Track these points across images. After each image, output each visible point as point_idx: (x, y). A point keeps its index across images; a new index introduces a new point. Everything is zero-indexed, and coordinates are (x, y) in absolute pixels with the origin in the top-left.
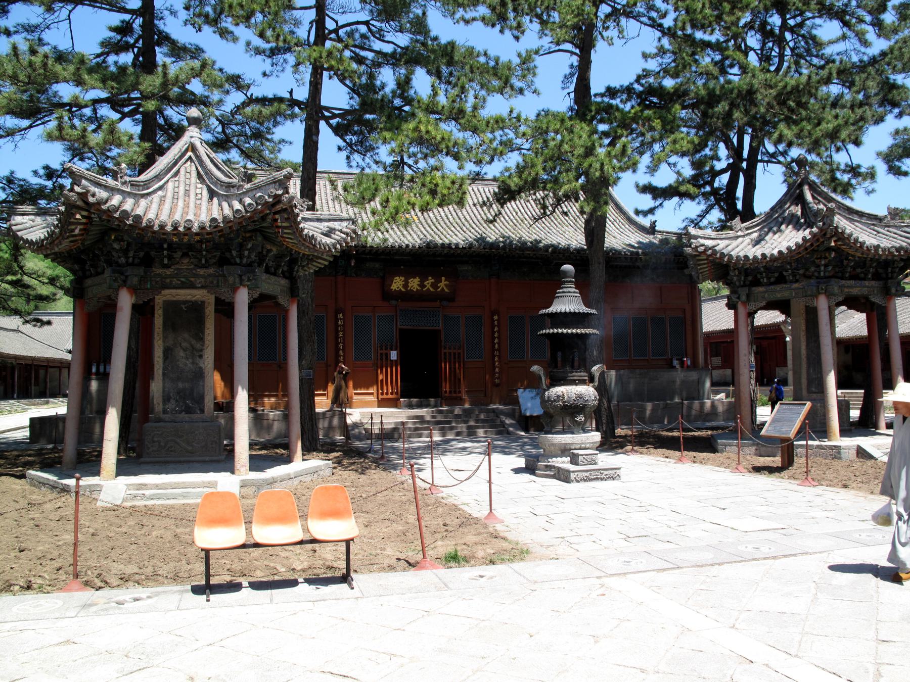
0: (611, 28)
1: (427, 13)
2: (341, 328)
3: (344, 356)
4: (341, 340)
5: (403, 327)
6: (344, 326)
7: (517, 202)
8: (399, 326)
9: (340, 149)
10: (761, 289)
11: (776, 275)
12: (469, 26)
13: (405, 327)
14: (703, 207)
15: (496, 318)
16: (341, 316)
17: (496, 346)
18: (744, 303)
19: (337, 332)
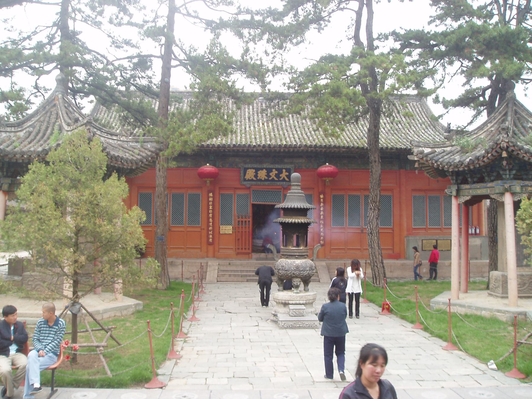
0: (250, 56)
1: (237, 38)
2: (211, 203)
3: (213, 223)
4: (210, 211)
5: (254, 203)
6: (213, 201)
7: (249, 141)
8: (252, 202)
9: (284, 84)
10: (467, 186)
11: (479, 176)
12: (391, 30)
13: (256, 203)
14: (473, 113)
15: (322, 196)
16: (211, 195)
17: (322, 217)
18: (457, 197)
19: (208, 206)
